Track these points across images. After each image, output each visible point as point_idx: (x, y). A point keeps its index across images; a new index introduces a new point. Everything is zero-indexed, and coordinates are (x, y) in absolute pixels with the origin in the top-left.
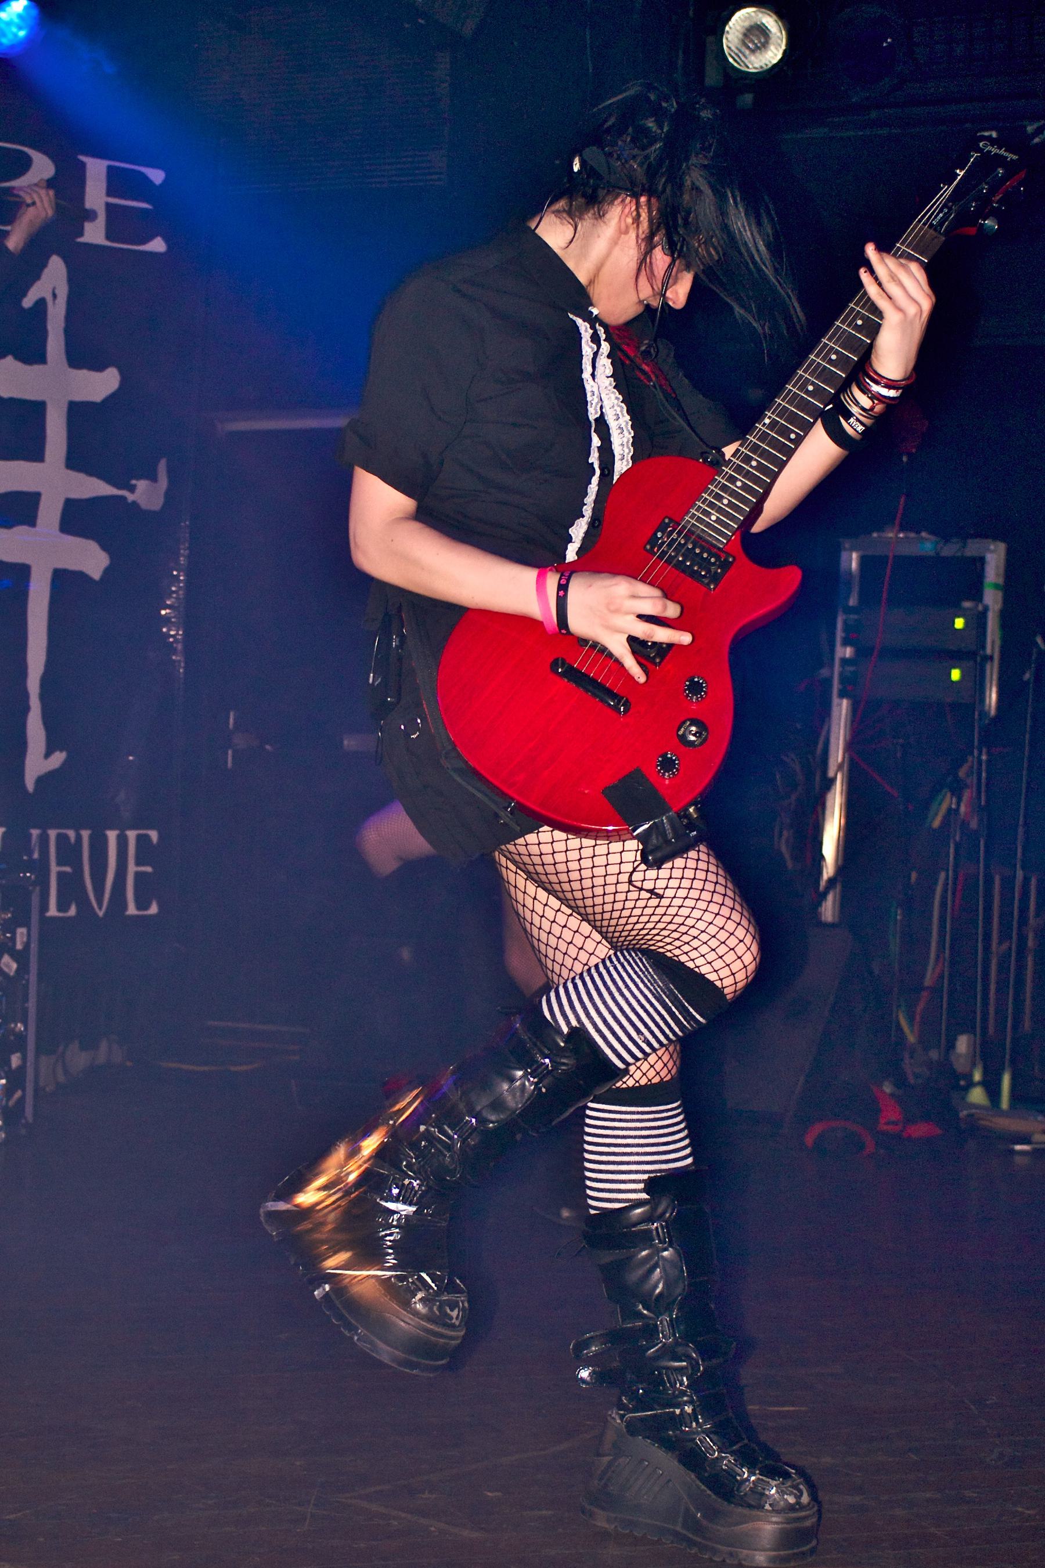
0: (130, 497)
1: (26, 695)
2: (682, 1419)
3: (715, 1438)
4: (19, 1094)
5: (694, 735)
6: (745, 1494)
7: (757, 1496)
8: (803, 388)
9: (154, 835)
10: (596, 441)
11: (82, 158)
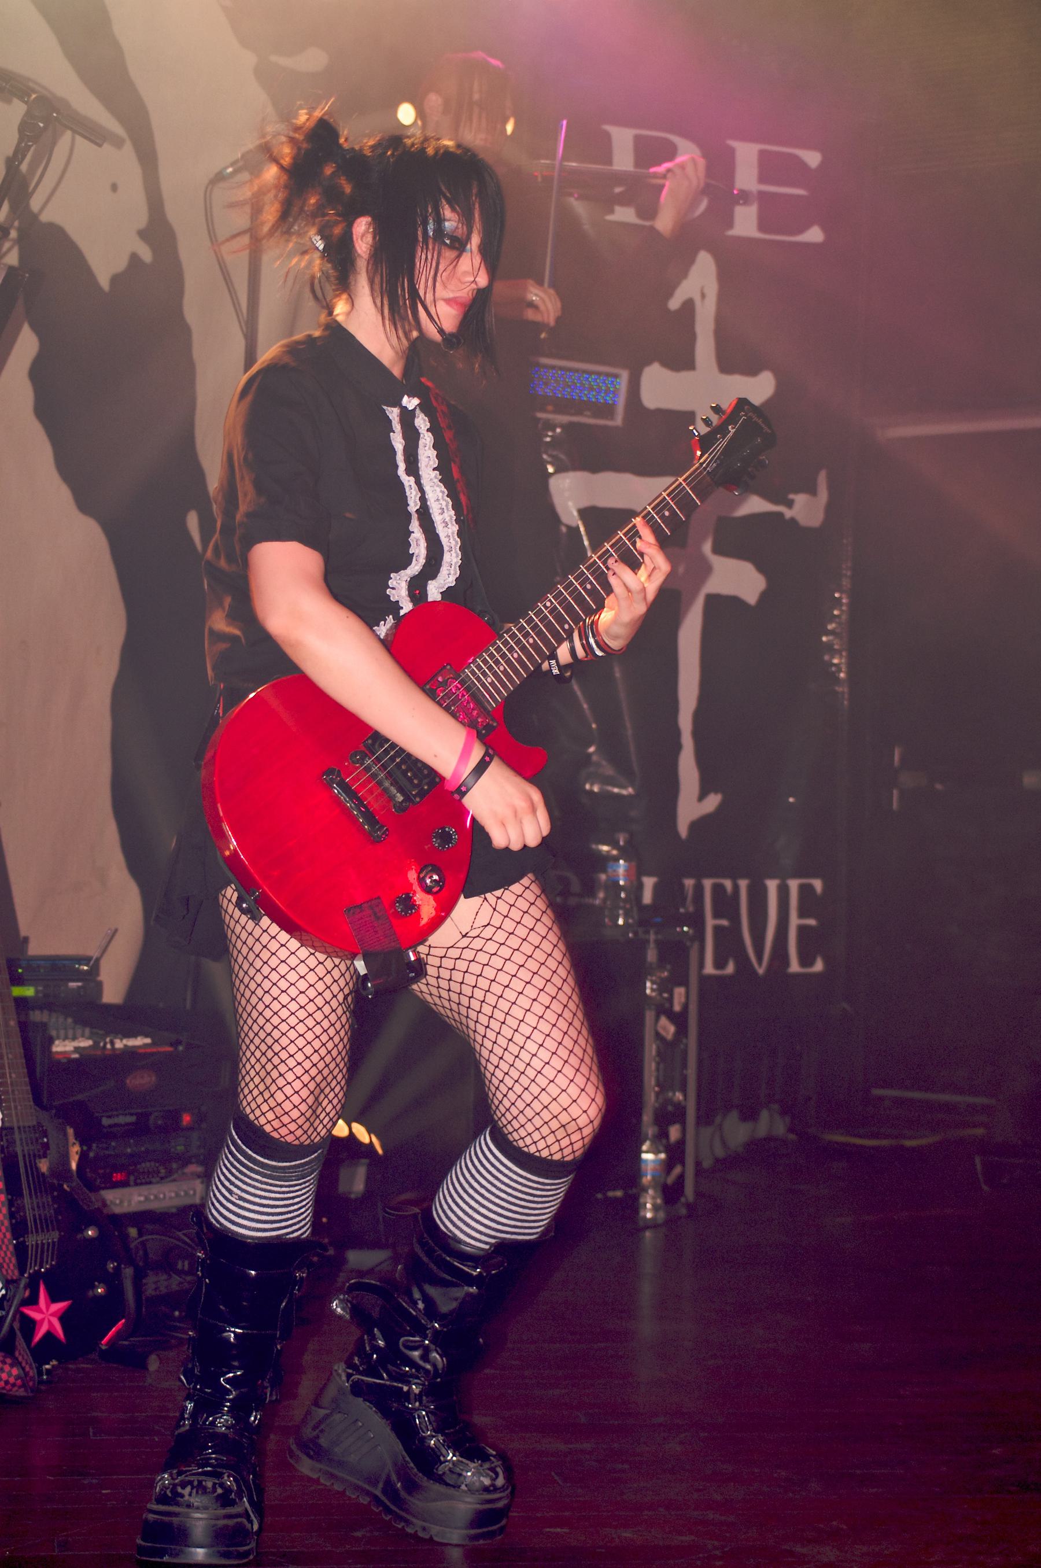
0: (788, 513)
1: (677, 733)
3: (432, 1418)
4: (677, 1170)
6: (444, 1473)
7: (455, 1476)
9: (818, 884)
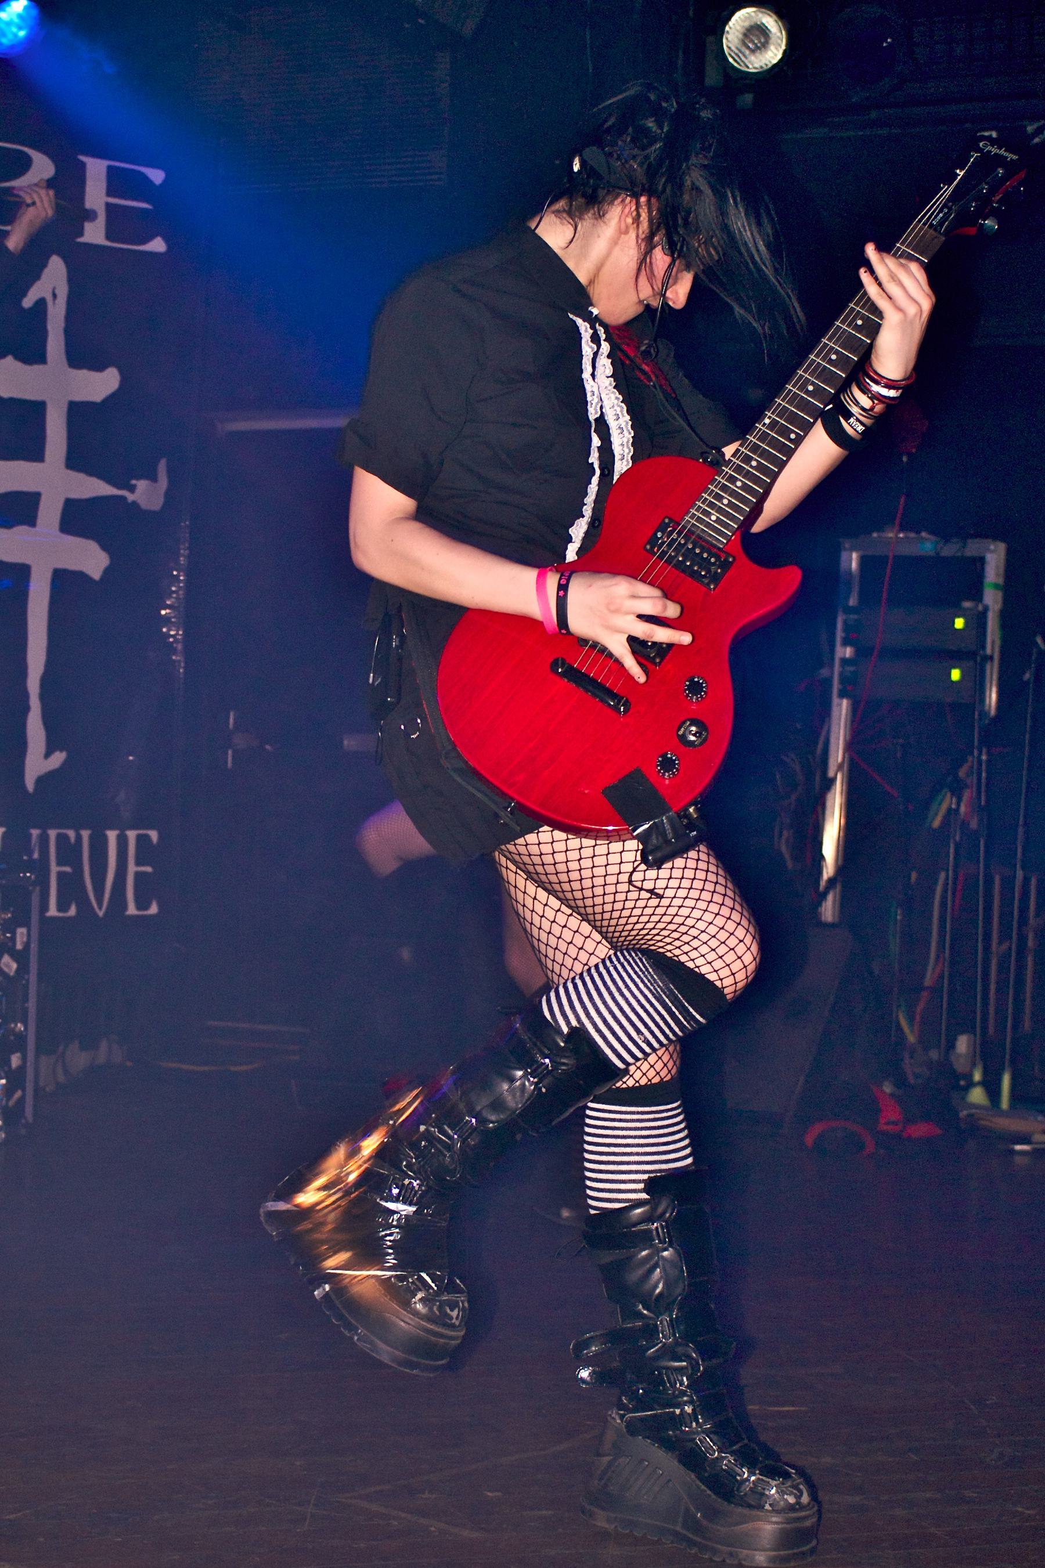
0: (130, 497)
1: (26, 695)
2: (682, 1419)
3: (715, 1438)
4: (19, 1094)
5: (694, 735)
6: (745, 1494)
7: (757, 1496)
8: (803, 388)
9: (154, 835)
10: (596, 441)
11: (82, 158)
